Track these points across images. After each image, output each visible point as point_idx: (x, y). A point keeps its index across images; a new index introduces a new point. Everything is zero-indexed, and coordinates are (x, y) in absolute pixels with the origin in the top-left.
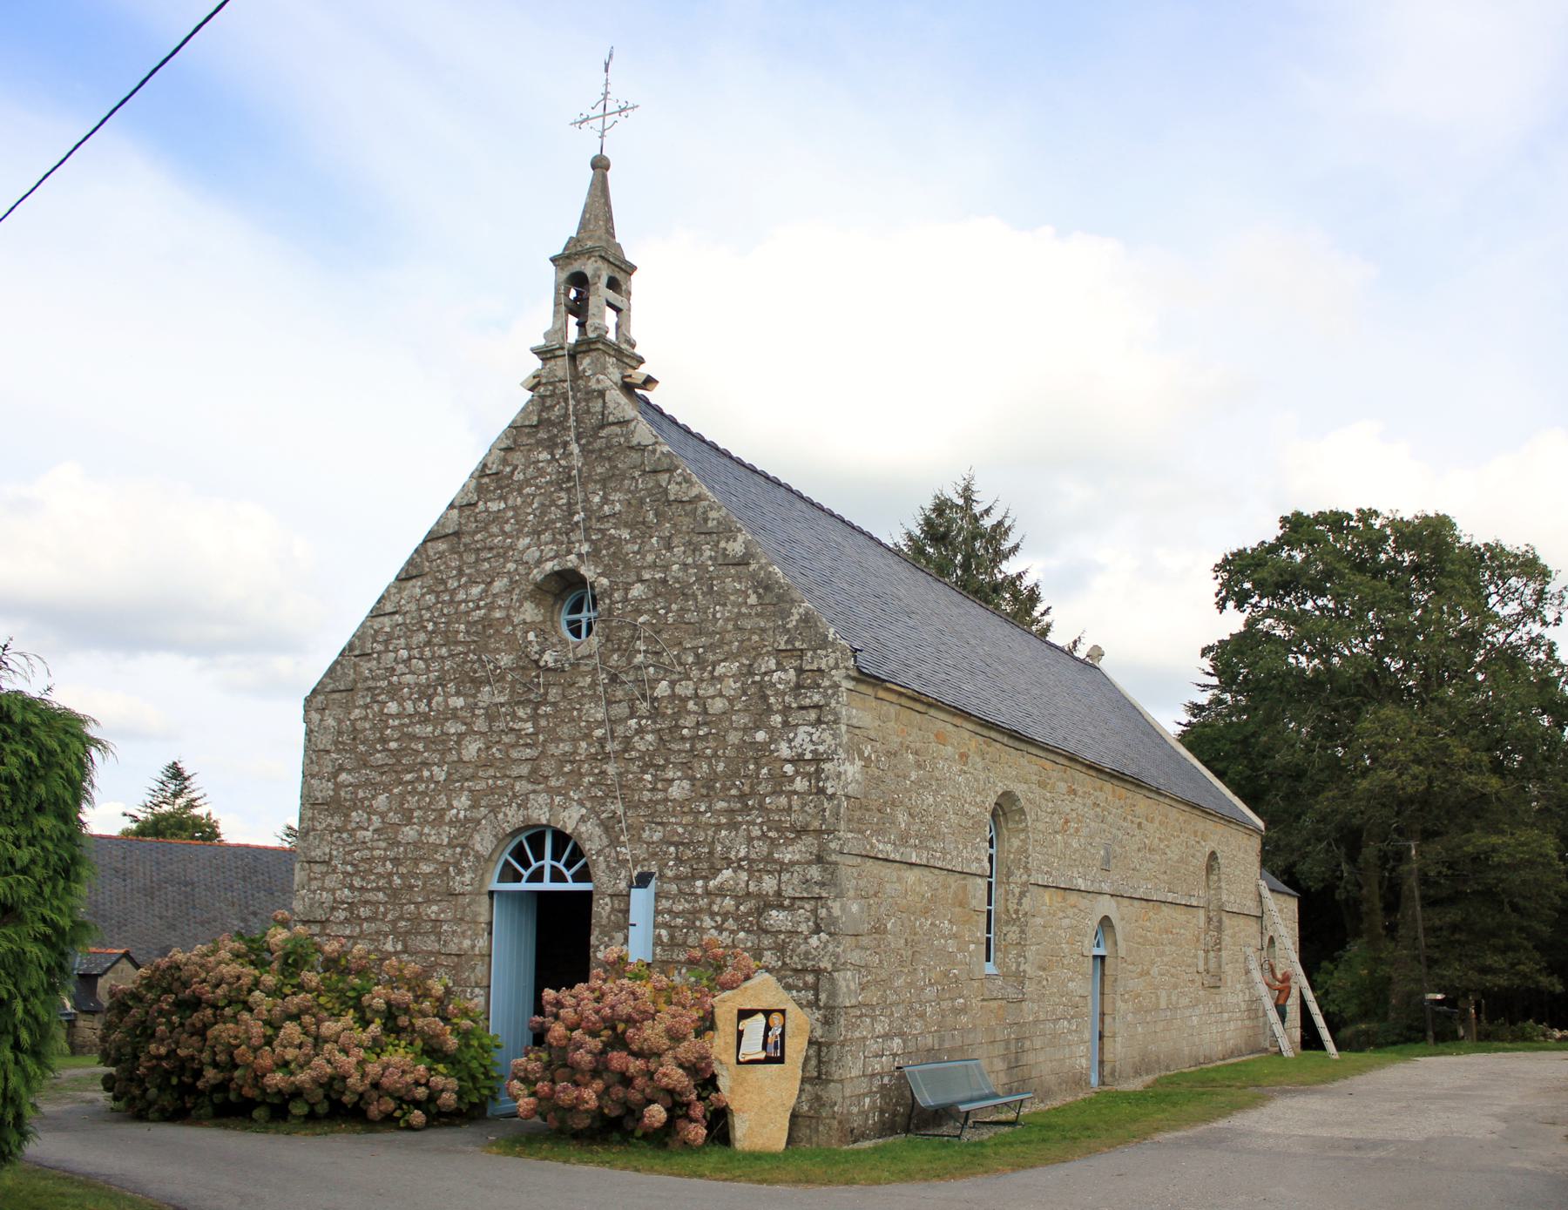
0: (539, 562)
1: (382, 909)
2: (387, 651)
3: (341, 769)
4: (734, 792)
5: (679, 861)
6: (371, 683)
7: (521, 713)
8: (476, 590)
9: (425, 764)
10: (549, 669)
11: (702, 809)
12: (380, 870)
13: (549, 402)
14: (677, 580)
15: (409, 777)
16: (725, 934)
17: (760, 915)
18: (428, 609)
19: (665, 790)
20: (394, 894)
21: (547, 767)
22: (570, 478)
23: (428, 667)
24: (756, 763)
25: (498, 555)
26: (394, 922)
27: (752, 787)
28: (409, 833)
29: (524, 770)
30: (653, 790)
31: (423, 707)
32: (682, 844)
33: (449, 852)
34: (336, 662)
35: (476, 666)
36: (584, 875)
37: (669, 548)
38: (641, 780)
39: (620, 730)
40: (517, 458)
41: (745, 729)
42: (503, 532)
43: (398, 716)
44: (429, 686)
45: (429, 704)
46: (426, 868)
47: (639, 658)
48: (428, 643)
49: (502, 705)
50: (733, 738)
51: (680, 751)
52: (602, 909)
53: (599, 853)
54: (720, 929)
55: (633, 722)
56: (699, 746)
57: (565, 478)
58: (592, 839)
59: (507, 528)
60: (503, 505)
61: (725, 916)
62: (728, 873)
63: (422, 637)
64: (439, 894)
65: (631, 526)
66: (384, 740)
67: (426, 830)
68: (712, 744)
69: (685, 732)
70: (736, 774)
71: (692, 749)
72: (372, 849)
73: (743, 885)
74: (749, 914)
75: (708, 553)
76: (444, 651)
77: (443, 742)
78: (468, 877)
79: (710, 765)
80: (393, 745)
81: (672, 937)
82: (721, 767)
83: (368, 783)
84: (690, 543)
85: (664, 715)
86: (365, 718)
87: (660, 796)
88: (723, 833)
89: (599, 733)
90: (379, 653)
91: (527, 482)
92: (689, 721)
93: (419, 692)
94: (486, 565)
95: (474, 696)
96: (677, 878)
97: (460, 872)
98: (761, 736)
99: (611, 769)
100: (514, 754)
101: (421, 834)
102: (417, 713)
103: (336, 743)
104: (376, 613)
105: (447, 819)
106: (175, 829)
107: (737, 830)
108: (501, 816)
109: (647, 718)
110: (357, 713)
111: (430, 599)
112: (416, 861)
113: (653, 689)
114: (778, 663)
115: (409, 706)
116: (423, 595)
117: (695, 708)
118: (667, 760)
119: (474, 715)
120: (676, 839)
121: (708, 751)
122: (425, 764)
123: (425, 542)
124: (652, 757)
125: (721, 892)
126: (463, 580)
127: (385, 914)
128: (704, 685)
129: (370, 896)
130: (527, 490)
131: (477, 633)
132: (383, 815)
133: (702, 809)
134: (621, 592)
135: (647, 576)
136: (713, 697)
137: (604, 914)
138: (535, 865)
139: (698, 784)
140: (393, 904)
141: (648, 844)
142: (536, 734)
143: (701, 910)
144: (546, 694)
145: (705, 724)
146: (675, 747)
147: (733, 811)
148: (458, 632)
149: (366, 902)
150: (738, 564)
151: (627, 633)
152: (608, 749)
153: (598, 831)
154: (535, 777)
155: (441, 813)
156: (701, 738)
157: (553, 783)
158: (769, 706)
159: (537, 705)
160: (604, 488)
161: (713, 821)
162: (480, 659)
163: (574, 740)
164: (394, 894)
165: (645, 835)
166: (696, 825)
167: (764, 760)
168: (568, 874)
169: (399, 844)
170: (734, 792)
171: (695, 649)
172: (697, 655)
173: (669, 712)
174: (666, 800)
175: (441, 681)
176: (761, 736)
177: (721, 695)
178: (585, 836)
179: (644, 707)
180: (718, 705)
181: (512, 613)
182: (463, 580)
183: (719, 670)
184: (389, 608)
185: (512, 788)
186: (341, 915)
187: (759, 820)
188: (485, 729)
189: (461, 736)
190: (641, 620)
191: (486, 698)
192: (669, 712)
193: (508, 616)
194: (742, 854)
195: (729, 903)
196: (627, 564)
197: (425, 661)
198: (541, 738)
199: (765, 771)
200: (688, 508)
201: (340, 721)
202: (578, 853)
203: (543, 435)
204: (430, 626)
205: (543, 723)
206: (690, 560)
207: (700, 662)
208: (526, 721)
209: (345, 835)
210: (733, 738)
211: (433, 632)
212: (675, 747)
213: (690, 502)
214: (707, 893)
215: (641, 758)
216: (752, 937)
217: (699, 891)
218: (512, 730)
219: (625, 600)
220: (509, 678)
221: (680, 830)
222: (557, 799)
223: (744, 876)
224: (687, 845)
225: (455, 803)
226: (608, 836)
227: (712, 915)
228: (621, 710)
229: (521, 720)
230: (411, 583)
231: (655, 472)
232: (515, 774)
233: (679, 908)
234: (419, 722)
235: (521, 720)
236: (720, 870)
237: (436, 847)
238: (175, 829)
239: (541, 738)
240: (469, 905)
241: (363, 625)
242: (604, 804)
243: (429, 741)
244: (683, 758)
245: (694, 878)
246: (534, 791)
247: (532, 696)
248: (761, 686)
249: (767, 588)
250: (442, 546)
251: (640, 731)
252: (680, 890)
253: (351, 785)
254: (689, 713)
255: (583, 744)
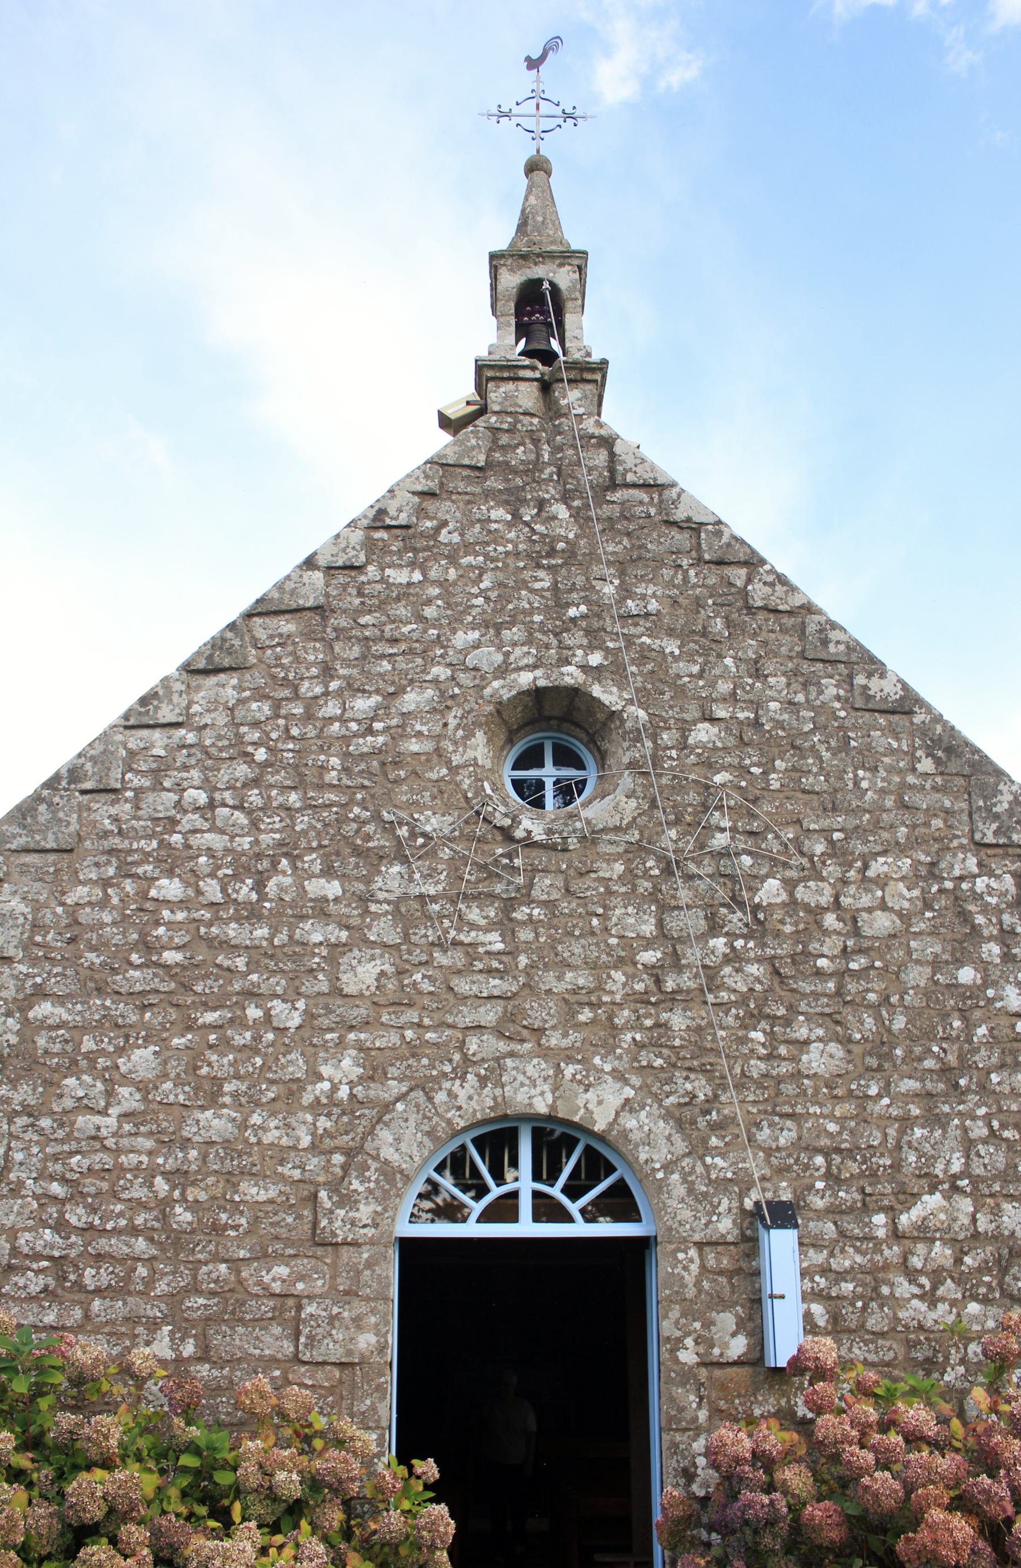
0: (503, 671)
1: (142, 1271)
2: (158, 786)
3: (40, 993)
4: (929, 1063)
5: (833, 1179)
6: (116, 842)
7: (474, 915)
8: (363, 704)
9: (251, 994)
10: (536, 845)
11: (873, 1091)
12: (138, 1192)
13: (504, 439)
14: (780, 724)
15: (210, 1017)
16: (942, 1307)
17: (1004, 1271)
18: (256, 724)
19: (794, 1059)
20: (174, 1243)
21: (539, 1012)
22: (552, 553)
23: (255, 824)
24: (964, 1019)
25: (411, 651)
26: (175, 1298)
27: (961, 1057)
28: (215, 1123)
29: (489, 1015)
30: (769, 1057)
31: (245, 891)
32: (838, 1150)
33: (314, 1163)
34: (37, 798)
35: (370, 828)
36: (620, 1203)
37: (758, 674)
38: (744, 1040)
39: (692, 955)
40: (445, 509)
41: (936, 964)
42: (421, 619)
43: (183, 904)
44: (259, 856)
45: (259, 886)
46: (252, 1191)
47: (720, 840)
48: (256, 782)
49: (434, 899)
50: (916, 976)
51: (816, 995)
52: (677, 1274)
53: (668, 1167)
54: (931, 1299)
55: (719, 943)
56: (852, 987)
57: (543, 552)
58: (650, 1141)
59: (429, 612)
60: (417, 576)
61: (937, 1276)
62: (934, 1201)
63: (242, 770)
64: (288, 1242)
65: (684, 635)
66: (148, 946)
67: (256, 1119)
68: (879, 985)
69: (822, 962)
70: (930, 1035)
71: (839, 992)
72: (118, 1151)
73: (966, 1221)
74: (983, 1269)
75: (832, 691)
76: (294, 798)
77: (295, 957)
78: (365, 1212)
79: (878, 1019)
80: (171, 957)
81: (835, 1318)
82: (899, 1023)
83: (109, 1023)
84: (796, 673)
85: (778, 934)
86: (104, 903)
87: (785, 1068)
88: (918, 1132)
89: (649, 957)
90: (139, 791)
91: (468, 548)
92: (831, 946)
93: (235, 863)
94: (386, 666)
95: (368, 881)
96: (834, 1211)
97: (348, 1200)
98: (967, 975)
99: (678, 1020)
100: (463, 986)
101: (243, 1126)
102: (229, 901)
103: (28, 945)
104: (136, 720)
105: (307, 1099)
106: (713, 837)
107: (944, 1127)
108: (441, 1097)
109: (746, 937)
110: (81, 893)
111: (260, 709)
112: (231, 1179)
113: (753, 890)
114: (980, 865)
115: (212, 890)
116: (241, 701)
117: (839, 926)
118: (790, 1008)
119: (367, 912)
120: (824, 1142)
121: (872, 997)
122: (251, 994)
123: (249, 615)
124: (763, 1001)
125: (924, 1233)
126: (334, 685)
127: (149, 1283)
128: (852, 889)
129: (115, 1245)
130: (465, 561)
131: (369, 773)
132: (144, 1088)
133: (873, 1091)
134: (675, 734)
135: (721, 713)
136: (870, 910)
137: (689, 1279)
138: (496, 1191)
139: (857, 1050)
140: (174, 1261)
141: (769, 1152)
142: (512, 953)
143: (886, 1267)
144: (530, 885)
145: (860, 951)
146: (806, 987)
147: (929, 1095)
148: (323, 768)
149: (99, 1258)
150: (893, 712)
151: (693, 797)
152: (670, 985)
153: (663, 1128)
154: (512, 1026)
155: (293, 1089)
156: (857, 975)
157: (554, 1040)
158: (975, 929)
159: (509, 905)
160: (622, 574)
161: (894, 1112)
162: (377, 817)
163: (593, 966)
164: (174, 1243)
165: (764, 1135)
166: (863, 1119)
167: (977, 1014)
168: (573, 1208)
169: (186, 1143)
170: (929, 1063)
171: (826, 833)
172: (831, 842)
173: (788, 929)
174: (797, 1076)
175: (289, 849)
176: (967, 975)
177: (883, 906)
178: (636, 1136)
179: (736, 919)
180: (882, 923)
181: (448, 746)
182: (334, 685)
183: (878, 867)
184: (166, 714)
185: (462, 1046)
186: (35, 1283)
187: (982, 1111)
188: (393, 937)
189: (337, 949)
190: (718, 779)
191: (394, 884)
192: (788, 929)
193: (438, 751)
194: (956, 1167)
195: (942, 1253)
196: (680, 692)
197: (249, 813)
198: (523, 960)
199: (982, 1030)
200: (789, 621)
201: (37, 907)
202: (595, 1165)
203: (493, 483)
204: (261, 755)
205: (525, 935)
206: (800, 698)
207: (834, 850)
208: (487, 930)
209: (45, 1123)
210: (916, 976)
211: (266, 764)
212: (806, 987)
213: (790, 613)
214: (896, 1235)
215: (743, 1000)
216: (993, 1311)
217: (881, 1233)
218: (456, 943)
219: (683, 745)
220: (446, 853)
221: (832, 1127)
222: (569, 1070)
223: (966, 1205)
224: (849, 1154)
225: (326, 1070)
226: (687, 1138)
227: (912, 1275)
228: (694, 921)
229: (473, 926)
230: (213, 680)
231: (720, 563)
232: (468, 1021)
233: (842, 1263)
234: (238, 919)
235: (473, 926)
236: (916, 1196)
237: (282, 1154)
238: (713, 837)
239: (523, 960)
240: (369, 1265)
241: (104, 737)
242: (670, 1081)
243: (260, 956)
244: (823, 1005)
245: (866, 1208)
246: (512, 1054)
247: (499, 888)
248: (956, 896)
249: (949, 750)
250: (287, 626)
251: (734, 958)
252: (842, 1233)
253: (62, 1025)
254: (826, 933)
255: (618, 976)
